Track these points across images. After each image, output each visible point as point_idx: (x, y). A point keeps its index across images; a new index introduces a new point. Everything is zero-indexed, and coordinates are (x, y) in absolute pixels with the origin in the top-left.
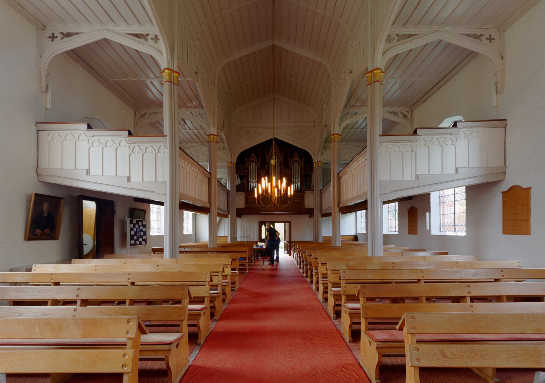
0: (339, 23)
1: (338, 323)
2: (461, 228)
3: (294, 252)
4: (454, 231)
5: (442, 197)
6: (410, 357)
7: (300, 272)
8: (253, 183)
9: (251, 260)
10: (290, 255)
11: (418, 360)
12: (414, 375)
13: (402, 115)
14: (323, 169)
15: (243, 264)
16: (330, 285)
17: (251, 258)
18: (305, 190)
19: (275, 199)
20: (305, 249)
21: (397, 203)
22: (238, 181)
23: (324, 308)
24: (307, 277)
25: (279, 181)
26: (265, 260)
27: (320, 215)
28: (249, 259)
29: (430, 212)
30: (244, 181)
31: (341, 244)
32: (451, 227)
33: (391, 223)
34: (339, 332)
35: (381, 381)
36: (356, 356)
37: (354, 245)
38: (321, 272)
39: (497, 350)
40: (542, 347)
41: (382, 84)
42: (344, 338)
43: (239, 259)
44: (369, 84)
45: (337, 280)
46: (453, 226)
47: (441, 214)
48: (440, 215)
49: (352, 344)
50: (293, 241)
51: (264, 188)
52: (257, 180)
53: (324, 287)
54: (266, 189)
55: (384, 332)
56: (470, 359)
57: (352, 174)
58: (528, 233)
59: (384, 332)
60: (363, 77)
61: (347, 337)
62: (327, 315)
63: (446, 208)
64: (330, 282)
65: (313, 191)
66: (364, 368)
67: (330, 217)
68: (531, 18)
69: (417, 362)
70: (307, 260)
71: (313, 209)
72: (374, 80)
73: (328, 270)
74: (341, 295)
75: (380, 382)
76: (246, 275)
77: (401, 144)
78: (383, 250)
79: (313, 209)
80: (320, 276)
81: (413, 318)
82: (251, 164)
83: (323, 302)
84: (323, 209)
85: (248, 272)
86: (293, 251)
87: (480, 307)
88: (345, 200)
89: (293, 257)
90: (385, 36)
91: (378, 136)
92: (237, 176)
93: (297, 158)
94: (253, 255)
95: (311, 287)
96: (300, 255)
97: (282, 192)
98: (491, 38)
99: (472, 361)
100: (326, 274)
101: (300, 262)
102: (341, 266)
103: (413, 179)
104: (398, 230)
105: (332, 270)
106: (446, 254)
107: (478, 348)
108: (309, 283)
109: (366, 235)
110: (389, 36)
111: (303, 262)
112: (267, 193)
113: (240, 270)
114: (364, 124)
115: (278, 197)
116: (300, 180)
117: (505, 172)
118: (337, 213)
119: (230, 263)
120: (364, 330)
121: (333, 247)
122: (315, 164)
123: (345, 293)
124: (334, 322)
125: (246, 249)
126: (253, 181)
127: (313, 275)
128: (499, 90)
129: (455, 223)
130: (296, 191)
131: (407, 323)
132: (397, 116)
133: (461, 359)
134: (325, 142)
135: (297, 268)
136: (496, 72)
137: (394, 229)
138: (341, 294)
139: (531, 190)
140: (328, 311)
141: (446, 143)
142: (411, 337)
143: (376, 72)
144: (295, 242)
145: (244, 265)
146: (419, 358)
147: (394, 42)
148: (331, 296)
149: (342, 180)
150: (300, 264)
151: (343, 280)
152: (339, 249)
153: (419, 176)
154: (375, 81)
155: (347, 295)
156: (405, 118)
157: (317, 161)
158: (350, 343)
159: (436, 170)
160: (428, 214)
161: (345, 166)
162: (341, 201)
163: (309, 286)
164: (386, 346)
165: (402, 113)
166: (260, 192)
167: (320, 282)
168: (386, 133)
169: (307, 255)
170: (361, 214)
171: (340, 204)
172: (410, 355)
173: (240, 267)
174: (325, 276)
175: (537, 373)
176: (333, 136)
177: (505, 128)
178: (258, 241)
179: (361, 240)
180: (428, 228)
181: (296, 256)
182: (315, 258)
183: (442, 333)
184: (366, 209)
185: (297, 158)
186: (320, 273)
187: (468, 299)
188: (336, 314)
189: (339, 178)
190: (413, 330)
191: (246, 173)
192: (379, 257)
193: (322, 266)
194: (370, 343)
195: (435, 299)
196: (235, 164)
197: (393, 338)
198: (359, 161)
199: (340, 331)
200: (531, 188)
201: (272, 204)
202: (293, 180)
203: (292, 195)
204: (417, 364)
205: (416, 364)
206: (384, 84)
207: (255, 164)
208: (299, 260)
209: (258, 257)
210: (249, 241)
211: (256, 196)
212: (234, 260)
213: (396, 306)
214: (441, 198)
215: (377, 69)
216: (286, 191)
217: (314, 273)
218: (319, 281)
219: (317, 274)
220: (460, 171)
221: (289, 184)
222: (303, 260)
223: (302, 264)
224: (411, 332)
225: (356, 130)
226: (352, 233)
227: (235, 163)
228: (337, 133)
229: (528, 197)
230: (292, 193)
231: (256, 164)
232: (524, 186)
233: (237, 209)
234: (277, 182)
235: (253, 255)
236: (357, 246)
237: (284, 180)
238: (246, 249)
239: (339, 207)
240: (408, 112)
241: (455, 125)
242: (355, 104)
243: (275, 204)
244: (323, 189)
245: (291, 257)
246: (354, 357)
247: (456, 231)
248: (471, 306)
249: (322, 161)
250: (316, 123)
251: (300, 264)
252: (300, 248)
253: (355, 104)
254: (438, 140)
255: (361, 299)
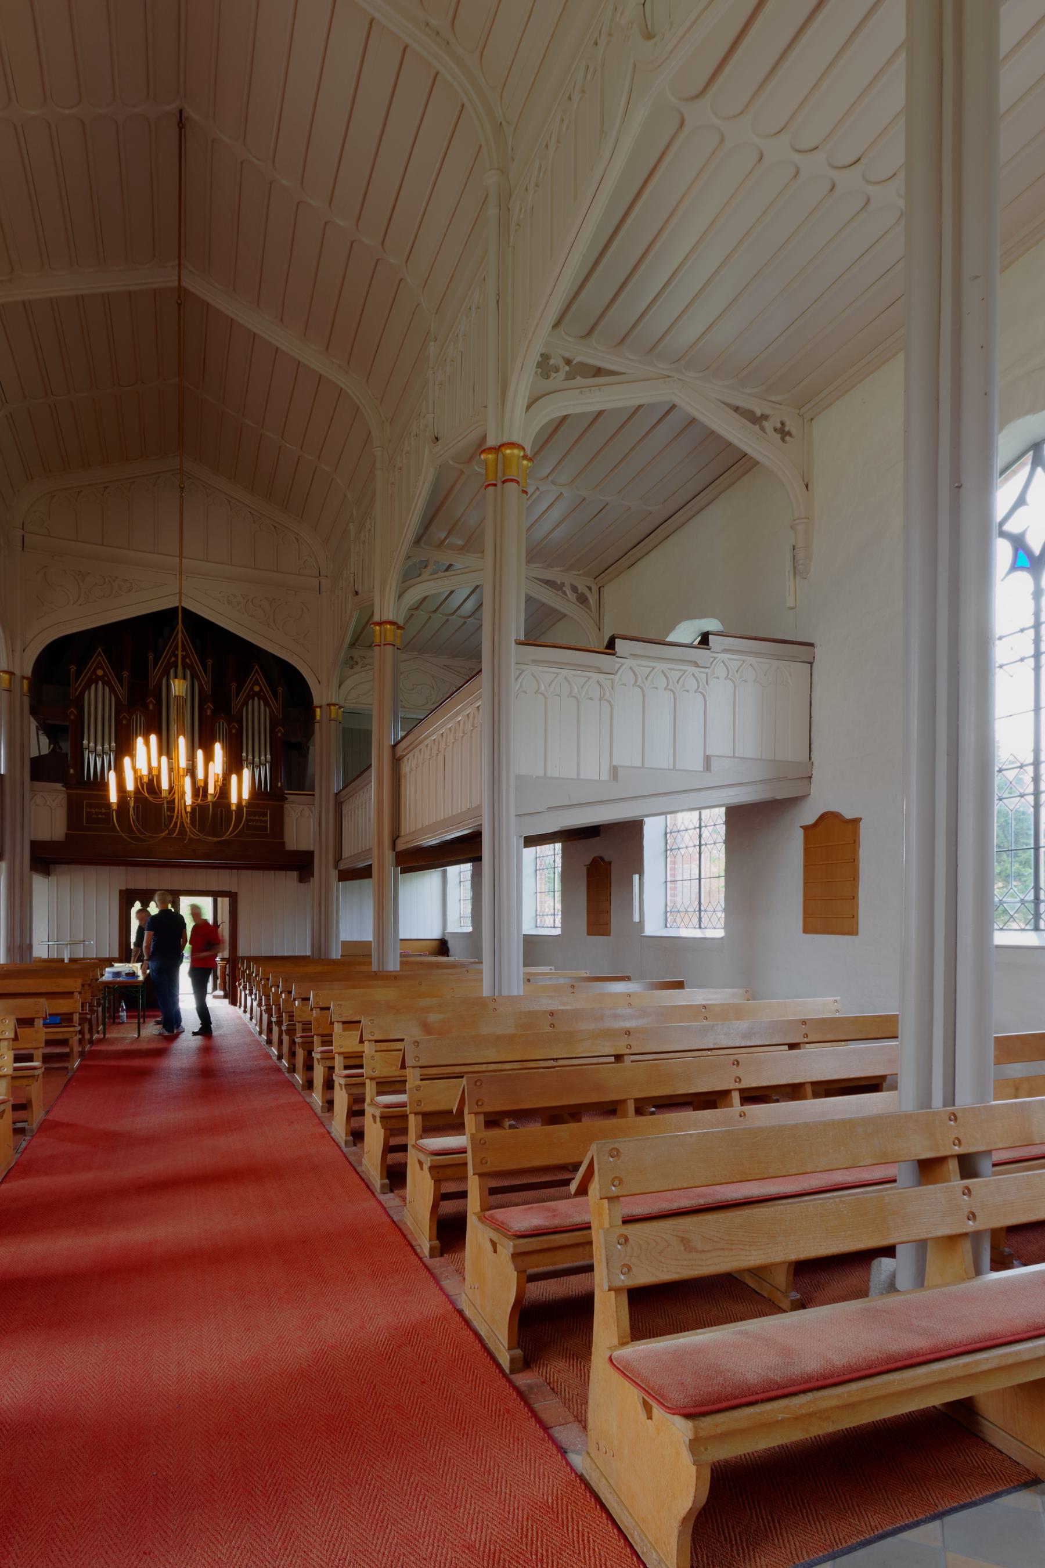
0: (401, 280)
1: (397, 1202)
2: (714, 920)
3: (247, 992)
4: (698, 926)
5: (671, 833)
6: (607, 1263)
7: (268, 1056)
8: (92, 752)
9: (91, 1025)
10: (234, 1002)
11: (625, 1270)
12: (617, 1312)
13: (575, 595)
14: (344, 729)
15: (60, 1037)
16: (370, 1089)
17: (89, 1016)
18: (286, 792)
19: (183, 812)
20: (285, 981)
21: (558, 846)
22: (40, 745)
23: (350, 1163)
24: (292, 1069)
25: (200, 754)
26: (142, 1020)
27: (334, 874)
28: (83, 1020)
29: (641, 874)
30: (62, 744)
31: (402, 963)
32: (690, 914)
33: (541, 902)
34: (400, 1230)
35: (522, 1351)
36: (451, 1294)
37: (439, 966)
38: (342, 1050)
39: (804, 1214)
40: (889, 1195)
41: (526, 492)
42: (414, 1243)
43: (45, 1019)
44: (488, 486)
45: (392, 1071)
46: (695, 911)
47: (668, 879)
48: (666, 882)
49: (438, 1259)
50: (243, 958)
51: (145, 772)
52: (113, 744)
53: (349, 1094)
54: (151, 781)
55: (532, 1208)
56: (747, 1247)
57: (435, 751)
58: (853, 931)
59: (532, 1208)
60: (469, 461)
61: (424, 1241)
62: (362, 1182)
63: (679, 866)
64: (372, 1079)
65: (313, 795)
66: (475, 1323)
67: (366, 882)
68: (864, 403)
69: (623, 1274)
70: (293, 1016)
71: (311, 854)
72: (504, 475)
73: (366, 1042)
74: (405, 1117)
75: (521, 1352)
76: (72, 1077)
77: (575, 676)
78: (524, 979)
79: (311, 854)
80: (338, 1062)
81: (615, 1153)
82: (90, 688)
83: (346, 1142)
84: (346, 854)
85: (80, 1066)
86: (245, 988)
87: (762, 1113)
88: (413, 829)
89: (242, 1008)
90: (534, 357)
91: (513, 643)
92: (34, 724)
93: (259, 685)
94: (99, 1005)
95: (308, 1099)
96: (268, 999)
97: (211, 790)
98: (784, 431)
99: (750, 1250)
100: (360, 1055)
101: (270, 1023)
102: (408, 1030)
103: (605, 777)
104: (562, 923)
105: (376, 1041)
106: (680, 985)
107: (764, 1217)
108: (300, 1088)
109: (474, 939)
110: (545, 357)
111: (279, 1023)
112: (156, 793)
113: (46, 1058)
114: (470, 606)
115: (193, 809)
116: (268, 756)
117: (810, 777)
118: (391, 869)
119: (10, 1034)
120: (478, 1209)
121: (375, 973)
122: (318, 710)
123: (418, 1109)
124: (384, 1203)
125: (72, 984)
126: (99, 748)
127: (315, 1062)
128: (800, 567)
129: (700, 903)
130: (257, 792)
131: (599, 1170)
132: (561, 594)
133: (727, 1249)
134: (352, 645)
135: (258, 1043)
136: (795, 520)
137: (549, 921)
138: (406, 1111)
139: (862, 824)
140: (363, 1168)
141: (683, 686)
142: (609, 1210)
143: (508, 451)
144: (250, 959)
145: (64, 1042)
146: (629, 1263)
147: (558, 379)
148: (375, 1122)
149: (406, 767)
150: (270, 1030)
151: (413, 1067)
152: (396, 977)
153: (620, 770)
154: (505, 478)
155: (426, 1115)
156: (582, 603)
157: (324, 703)
158: (432, 1256)
159: (660, 758)
160: (636, 877)
161: (413, 725)
162: (403, 833)
163: (301, 1099)
164: (538, 1248)
165: (574, 589)
166: (130, 786)
167: (339, 1080)
168: (533, 639)
169: (294, 1000)
170: (460, 873)
171: (399, 842)
172: (607, 1259)
173: (49, 1050)
174: (354, 1061)
175: (875, 1263)
176: (378, 628)
177: (811, 667)
178: (117, 955)
179: (457, 954)
180: (637, 919)
181: (255, 1003)
182: (322, 1009)
183: (685, 1186)
184: (476, 859)
185: (259, 685)
186: (339, 1054)
187: (736, 1097)
188: (388, 1177)
189: (396, 762)
190: (613, 1188)
191: (72, 717)
192: (513, 1000)
193: (344, 1030)
194: (494, 1244)
195: (653, 1109)
196: (25, 681)
197: (556, 1222)
198: (458, 714)
199: (400, 1225)
200: (859, 820)
201: (173, 831)
202: (244, 754)
203: (244, 803)
204: (623, 1281)
205: (624, 1280)
206: (530, 493)
207: (107, 689)
208: (265, 1016)
209: (118, 1012)
210: (84, 959)
211: (113, 797)
212: (25, 1022)
213: (563, 1131)
214: (668, 835)
215: (511, 445)
216: (224, 791)
217: (316, 1056)
218: (335, 1078)
219: (328, 1056)
220: (714, 765)
221: (234, 765)
222: (280, 1016)
223: (275, 1029)
224: (609, 1195)
225: (448, 620)
226: (432, 931)
227: (26, 678)
228: (391, 618)
229: (855, 843)
230: (246, 795)
231: (112, 690)
232: (848, 815)
233: (33, 844)
234: (192, 758)
235: (99, 1005)
236: (448, 971)
237: (218, 749)
238: (72, 984)
239: (394, 850)
240: (590, 588)
241: (705, 639)
242: (446, 538)
243: (183, 831)
244: (344, 793)
245: (237, 1008)
246: (447, 1296)
247: (703, 926)
248: (743, 1115)
249: (342, 704)
250: (324, 580)
251: (270, 1030)
252: (268, 979)
253: (446, 538)
254: (666, 676)
255: (469, 1120)
